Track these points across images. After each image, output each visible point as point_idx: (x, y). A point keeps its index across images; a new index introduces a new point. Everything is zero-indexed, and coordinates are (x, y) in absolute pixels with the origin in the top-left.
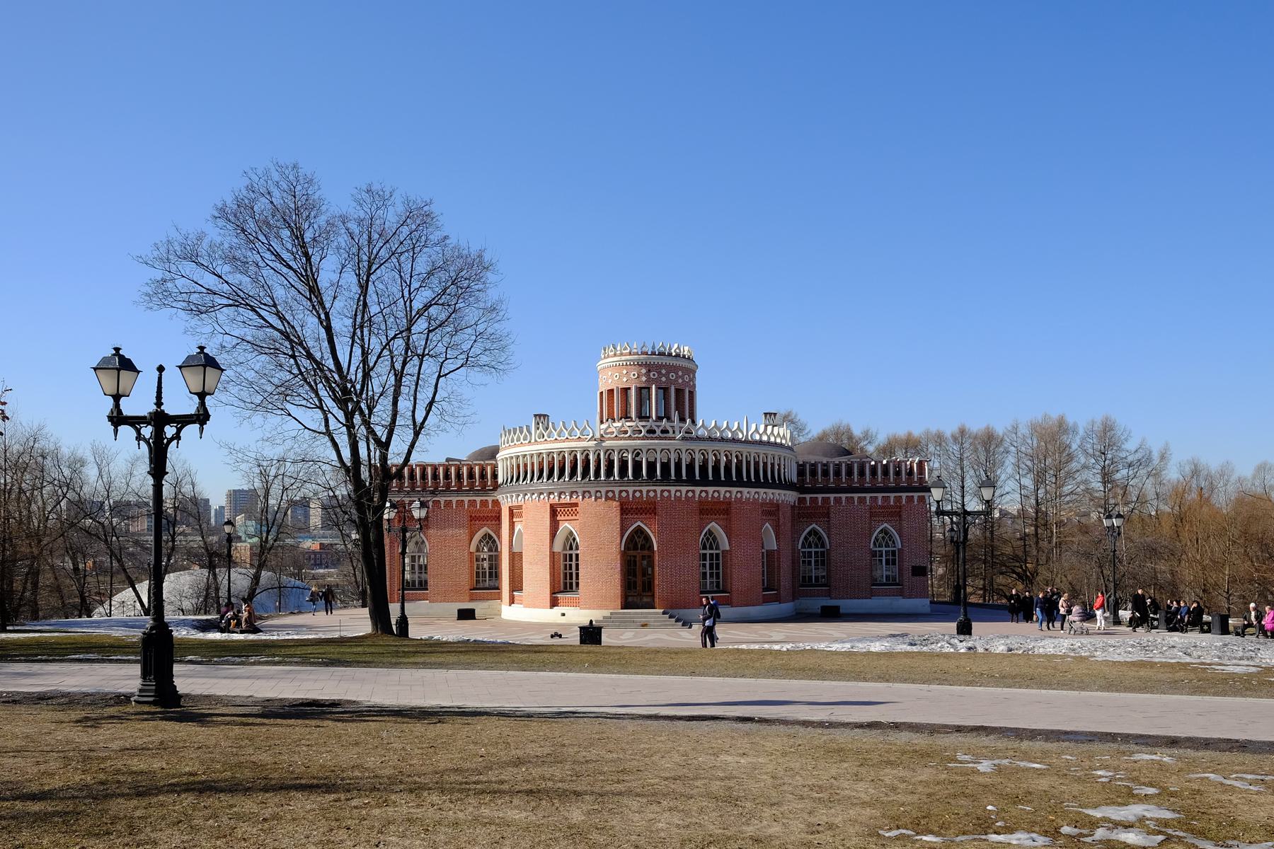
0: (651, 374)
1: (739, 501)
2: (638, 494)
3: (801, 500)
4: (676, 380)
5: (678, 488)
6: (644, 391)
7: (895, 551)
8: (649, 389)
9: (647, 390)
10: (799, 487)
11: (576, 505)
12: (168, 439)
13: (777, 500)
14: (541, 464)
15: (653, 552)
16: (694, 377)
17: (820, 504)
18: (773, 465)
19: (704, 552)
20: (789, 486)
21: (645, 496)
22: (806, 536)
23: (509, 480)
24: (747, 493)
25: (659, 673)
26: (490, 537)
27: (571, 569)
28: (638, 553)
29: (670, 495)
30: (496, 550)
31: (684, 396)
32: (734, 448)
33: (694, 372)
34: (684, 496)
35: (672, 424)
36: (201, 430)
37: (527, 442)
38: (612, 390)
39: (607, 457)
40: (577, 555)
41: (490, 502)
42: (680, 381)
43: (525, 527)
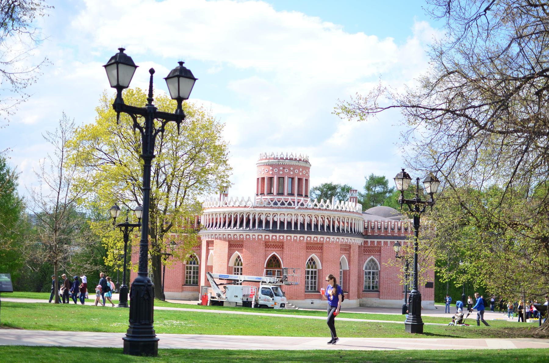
0: (285, 170)
1: (328, 243)
3: (366, 242)
4: (298, 174)
5: (296, 235)
10: (365, 235)
11: (213, 241)
13: (349, 243)
14: (225, 218)
16: (309, 171)
17: (376, 245)
18: (351, 224)
19: (308, 270)
20: (359, 234)
21: (278, 238)
23: (207, 226)
24: (333, 239)
29: (291, 238)
30: (198, 263)
31: (302, 183)
32: (326, 213)
34: (298, 239)
37: (218, 206)
38: (264, 178)
40: (241, 269)
42: (301, 174)
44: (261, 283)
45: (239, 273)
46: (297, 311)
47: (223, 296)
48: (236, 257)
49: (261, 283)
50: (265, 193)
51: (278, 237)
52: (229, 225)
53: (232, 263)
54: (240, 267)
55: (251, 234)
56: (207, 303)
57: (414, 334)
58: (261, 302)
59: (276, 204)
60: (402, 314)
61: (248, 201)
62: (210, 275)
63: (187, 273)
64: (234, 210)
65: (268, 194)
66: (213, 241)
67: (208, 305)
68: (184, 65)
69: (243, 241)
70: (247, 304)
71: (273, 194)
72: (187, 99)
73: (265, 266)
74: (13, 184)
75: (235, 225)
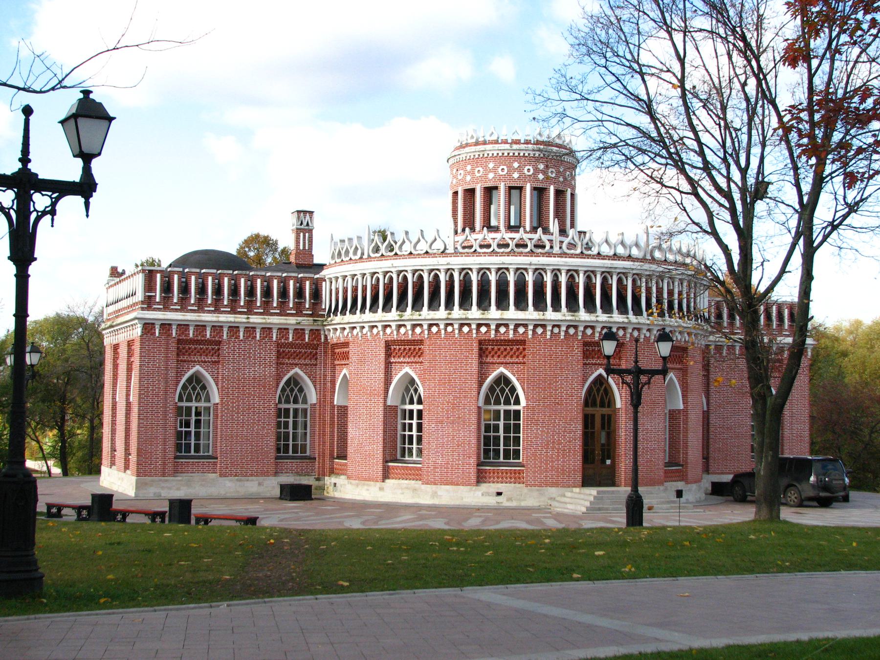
6: (515, 193)
7: (209, 408)
8: (521, 189)
9: (518, 191)
12: (38, 212)
15: (616, 410)
22: (184, 384)
27: (411, 443)
28: (598, 411)
33: (574, 167)
35: (550, 237)
36: (87, 205)
39: (462, 278)
40: (420, 412)
64: (409, 264)
68: (92, 96)
72: (99, 154)
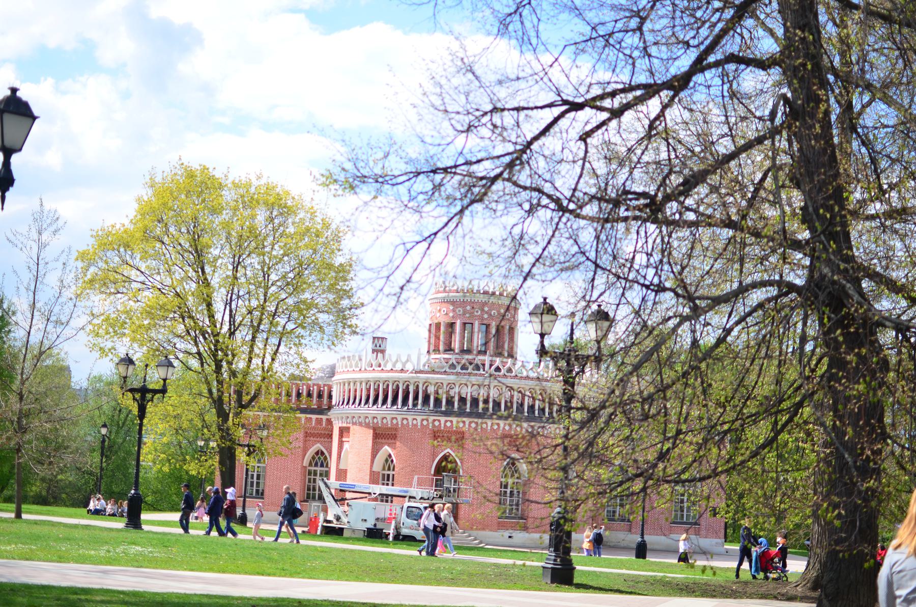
2: (395, 421)
11: (348, 428)
25: (404, 582)
26: (323, 453)
30: (327, 466)
41: (324, 421)
43: (351, 447)
44: (407, 499)
45: (390, 483)
46: (471, 549)
47: (344, 519)
48: (386, 456)
49: (407, 499)
50: (441, 348)
51: (443, 422)
52: (375, 401)
53: (378, 466)
54: (391, 473)
55: (410, 418)
56: (317, 529)
57: (554, 585)
58: (405, 531)
59: (464, 368)
60: (634, 558)
61: (407, 361)
62: (325, 484)
63: (309, 481)
64: (384, 375)
65: (445, 351)
66: (348, 428)
67: (319, 533)
69: (396, 430)
70: (374, 534)
71: (453, 350)
72: (20, 150)
73: (433, 472)
74: (8, 324)
75: (385, 401)
